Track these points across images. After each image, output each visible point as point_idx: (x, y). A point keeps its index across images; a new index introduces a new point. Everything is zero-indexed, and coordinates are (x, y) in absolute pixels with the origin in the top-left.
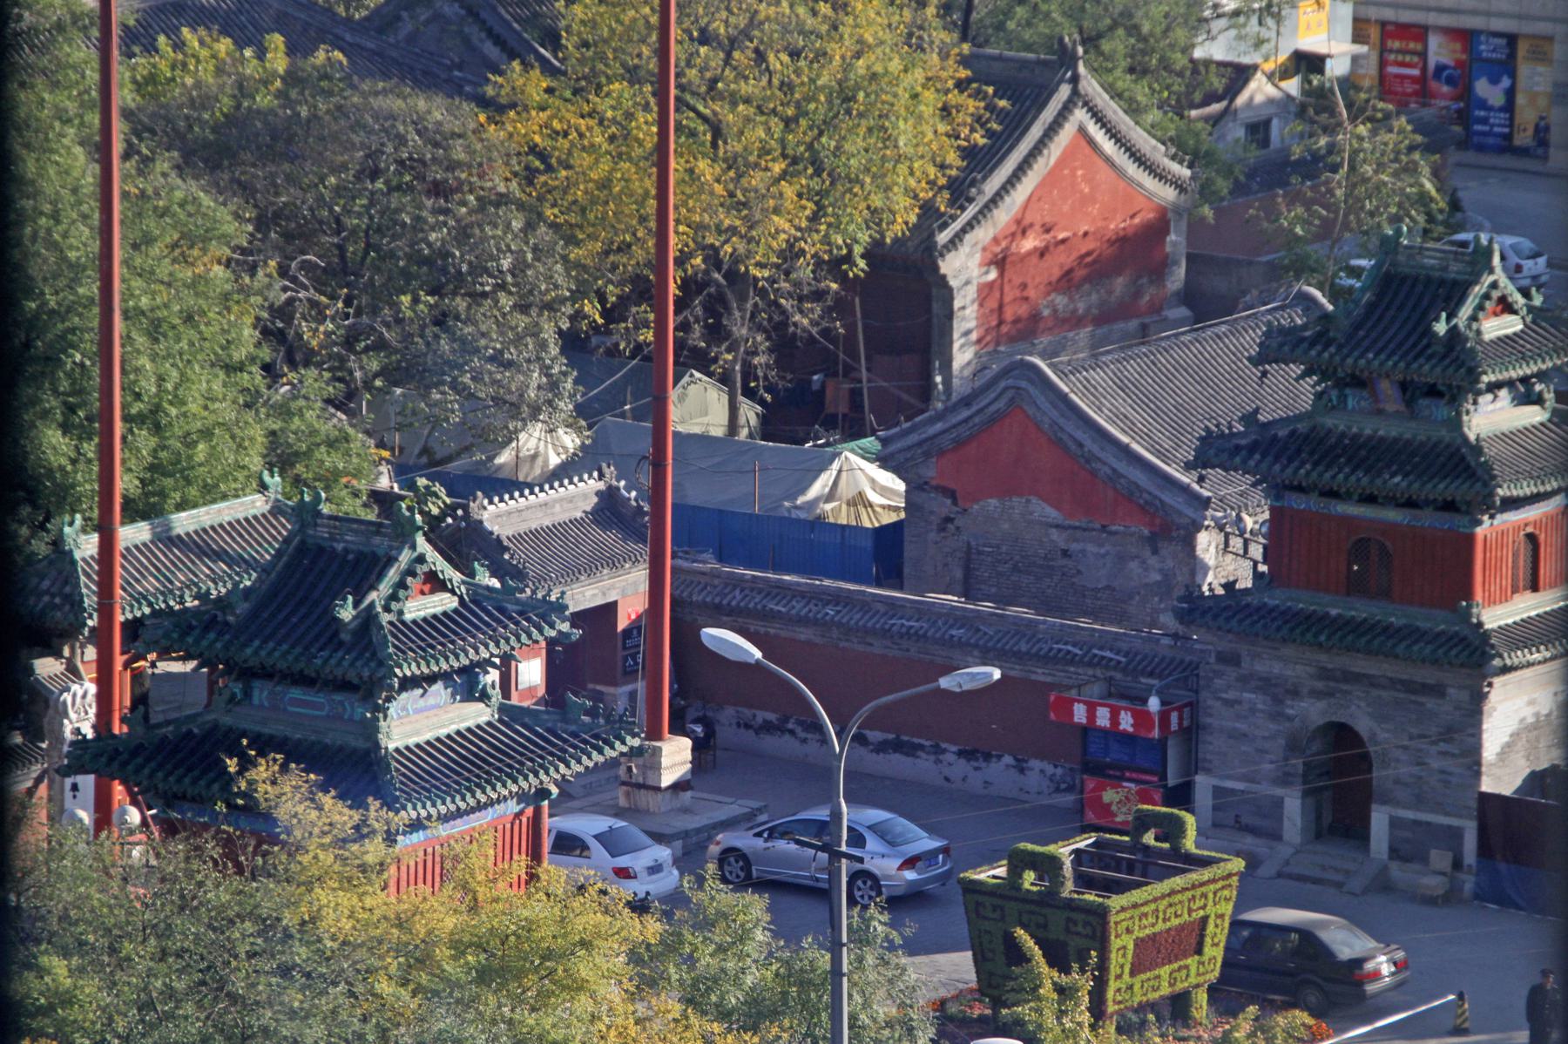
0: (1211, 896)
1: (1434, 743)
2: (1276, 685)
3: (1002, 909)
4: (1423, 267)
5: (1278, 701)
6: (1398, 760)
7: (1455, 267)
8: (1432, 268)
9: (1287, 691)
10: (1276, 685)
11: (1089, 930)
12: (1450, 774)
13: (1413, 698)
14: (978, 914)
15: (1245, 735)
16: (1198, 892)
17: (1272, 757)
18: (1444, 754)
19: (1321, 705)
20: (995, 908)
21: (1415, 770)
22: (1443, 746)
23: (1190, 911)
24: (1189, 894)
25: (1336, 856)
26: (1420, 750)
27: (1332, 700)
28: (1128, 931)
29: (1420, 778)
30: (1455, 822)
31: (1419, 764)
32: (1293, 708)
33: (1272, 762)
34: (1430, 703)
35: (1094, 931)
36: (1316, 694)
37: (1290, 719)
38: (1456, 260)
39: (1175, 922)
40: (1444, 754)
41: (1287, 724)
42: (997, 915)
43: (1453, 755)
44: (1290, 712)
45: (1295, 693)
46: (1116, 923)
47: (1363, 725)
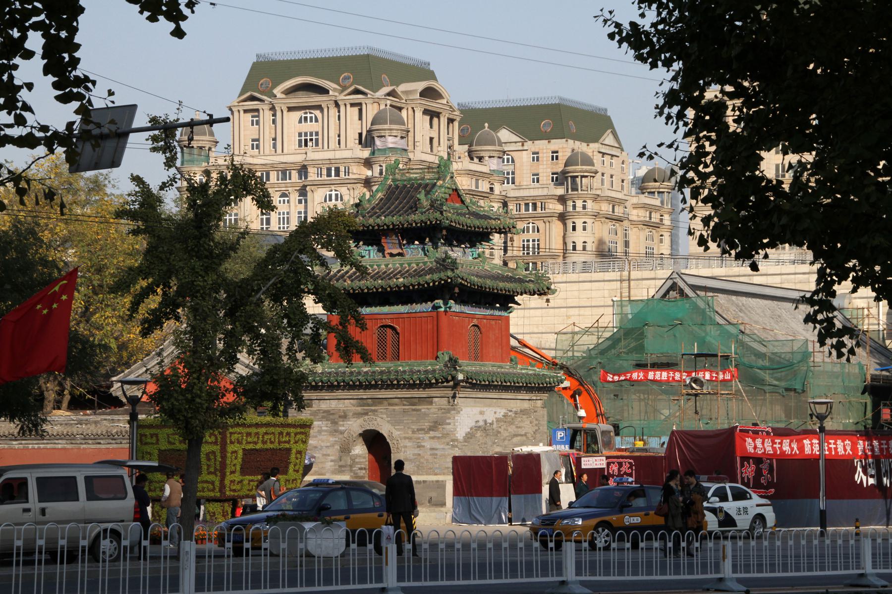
0: (293, 435)
1: (427, 432)
2: (333, 414)
3: (157, 435)
4: (410, 179)
5: (335, 423)
6: (406, 447)
7: (428, 176)
8: (416, 179)
9: (340, 417)
10: (333, 414)
11: (213, 439)
12: (436, 449)
13: (414, 407)
14: (141, 441)
15: (316, 447)
16: (285, 430)
17: (333, 458)
18: (433, 438)
19: (360, 421)
20: (152, 436)
21: (416, 451)
22: (432, 434)
23: (280, 442)
24: (279, 430)
25: (337, 165)
26: (419, 438)
27: (366, 417)
28: (239, 442)
29: (419, 455)
30: (440, 478)
31: (419, 447)
32: (344, 426)
33: (332, 461)
34: (423, 408)
35: (216, 439)
36: (358, 415)
37: (342, 433)
38: (428, 172)
39: (269, 446)
40: (433, 438)
41: (341, 436)
42: (154, 440)
43: (439, 438)
44: (341, 428)
45: (344, 417)
46: (231, 433)
47: (385, 429)
